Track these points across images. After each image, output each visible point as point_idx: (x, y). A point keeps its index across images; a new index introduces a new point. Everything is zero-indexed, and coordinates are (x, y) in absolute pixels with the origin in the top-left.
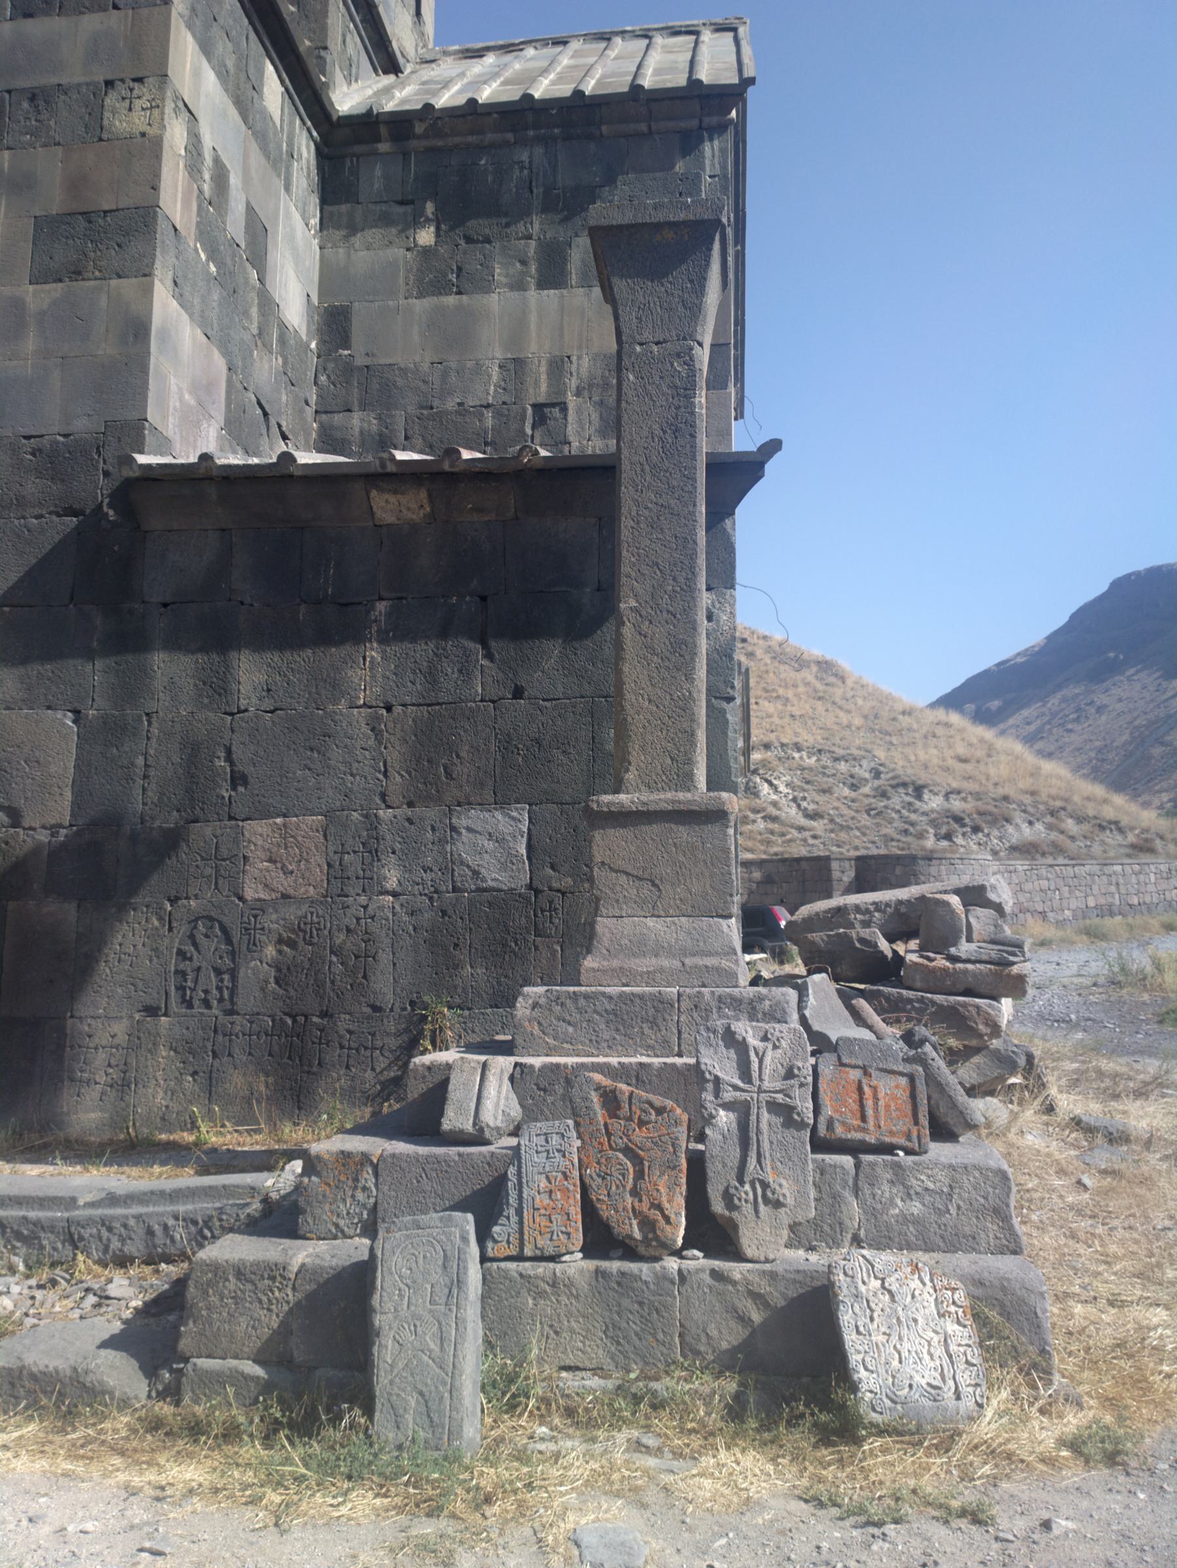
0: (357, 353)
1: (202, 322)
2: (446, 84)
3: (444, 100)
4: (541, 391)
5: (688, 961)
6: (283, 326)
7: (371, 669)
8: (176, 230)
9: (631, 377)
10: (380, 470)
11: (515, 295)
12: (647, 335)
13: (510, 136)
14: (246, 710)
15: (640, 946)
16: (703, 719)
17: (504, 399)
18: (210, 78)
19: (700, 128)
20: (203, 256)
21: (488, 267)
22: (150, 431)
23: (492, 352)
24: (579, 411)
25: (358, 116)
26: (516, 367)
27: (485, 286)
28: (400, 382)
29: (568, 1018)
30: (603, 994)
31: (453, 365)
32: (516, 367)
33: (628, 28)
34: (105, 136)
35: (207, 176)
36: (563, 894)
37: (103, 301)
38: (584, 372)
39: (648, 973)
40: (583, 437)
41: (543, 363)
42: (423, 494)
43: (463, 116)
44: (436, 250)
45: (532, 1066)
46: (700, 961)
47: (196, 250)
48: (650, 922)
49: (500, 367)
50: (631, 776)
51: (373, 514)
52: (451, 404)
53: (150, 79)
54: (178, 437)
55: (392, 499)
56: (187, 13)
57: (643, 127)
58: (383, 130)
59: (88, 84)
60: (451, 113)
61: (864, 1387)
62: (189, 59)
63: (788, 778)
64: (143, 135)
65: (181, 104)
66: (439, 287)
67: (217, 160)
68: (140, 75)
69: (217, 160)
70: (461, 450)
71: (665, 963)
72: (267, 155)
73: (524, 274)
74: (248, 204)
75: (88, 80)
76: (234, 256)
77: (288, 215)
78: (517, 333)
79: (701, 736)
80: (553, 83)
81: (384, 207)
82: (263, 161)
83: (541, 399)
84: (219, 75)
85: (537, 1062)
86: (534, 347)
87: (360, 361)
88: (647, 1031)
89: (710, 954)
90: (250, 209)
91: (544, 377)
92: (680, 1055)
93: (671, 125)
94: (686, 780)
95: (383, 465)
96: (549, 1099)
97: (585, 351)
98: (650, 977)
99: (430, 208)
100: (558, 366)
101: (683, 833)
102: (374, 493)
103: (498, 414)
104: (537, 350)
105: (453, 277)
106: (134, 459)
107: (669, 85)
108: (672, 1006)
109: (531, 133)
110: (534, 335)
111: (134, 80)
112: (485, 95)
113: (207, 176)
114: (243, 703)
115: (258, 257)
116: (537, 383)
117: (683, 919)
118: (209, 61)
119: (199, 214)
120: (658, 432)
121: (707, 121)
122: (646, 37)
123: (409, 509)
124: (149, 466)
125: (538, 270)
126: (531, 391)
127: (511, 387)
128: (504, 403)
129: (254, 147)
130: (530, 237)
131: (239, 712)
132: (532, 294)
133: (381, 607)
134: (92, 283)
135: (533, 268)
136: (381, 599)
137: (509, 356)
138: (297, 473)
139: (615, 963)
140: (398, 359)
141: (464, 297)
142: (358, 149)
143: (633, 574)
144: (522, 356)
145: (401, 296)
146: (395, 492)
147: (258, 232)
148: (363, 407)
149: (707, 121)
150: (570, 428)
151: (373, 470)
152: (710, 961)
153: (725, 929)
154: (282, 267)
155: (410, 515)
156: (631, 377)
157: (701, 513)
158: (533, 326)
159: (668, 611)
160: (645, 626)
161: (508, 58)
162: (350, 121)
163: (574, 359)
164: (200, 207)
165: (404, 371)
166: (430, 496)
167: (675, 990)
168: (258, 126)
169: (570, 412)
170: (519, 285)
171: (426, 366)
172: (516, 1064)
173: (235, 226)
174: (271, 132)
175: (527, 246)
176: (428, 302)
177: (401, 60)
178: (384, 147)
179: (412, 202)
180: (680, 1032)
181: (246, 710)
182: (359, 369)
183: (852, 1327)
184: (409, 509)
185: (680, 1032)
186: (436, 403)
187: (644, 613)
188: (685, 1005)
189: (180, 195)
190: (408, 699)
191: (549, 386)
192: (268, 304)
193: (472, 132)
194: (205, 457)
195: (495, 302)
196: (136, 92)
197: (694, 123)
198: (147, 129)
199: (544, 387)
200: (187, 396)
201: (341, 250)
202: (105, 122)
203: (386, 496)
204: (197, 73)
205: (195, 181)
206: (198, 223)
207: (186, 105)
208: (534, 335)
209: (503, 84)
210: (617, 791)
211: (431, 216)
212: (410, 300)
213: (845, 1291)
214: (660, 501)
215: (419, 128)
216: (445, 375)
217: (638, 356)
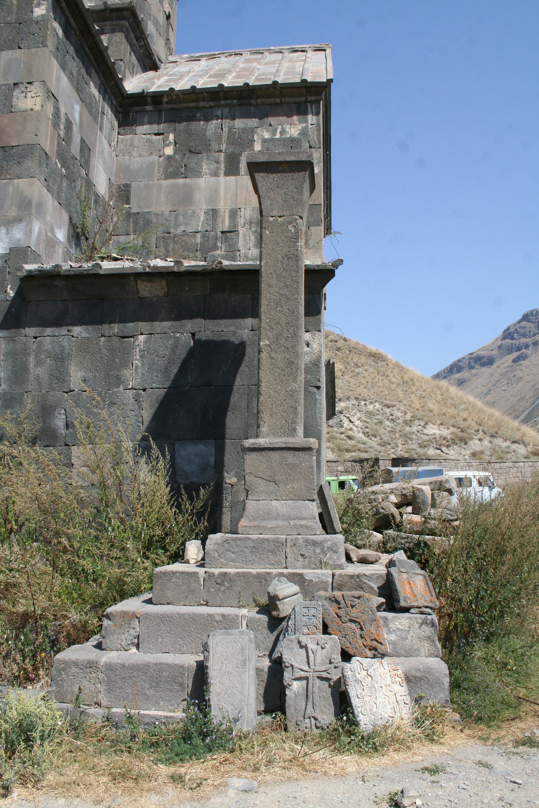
0: (134, 207)
1: (58, 197)
2: (181, 76)
3: (179, 86)
4: (226, 226)
5: (292, 522)
6: (97, 195)
7: (136, 370)
8: (47, 154)
9: (267, 232)
10: (142, 271)
11: (214, 179)
12: (275, 213)
13: (212, 104)
14: (74, 391)
15: (268, 515)
16: (302, 402)
17: (207, 229)
18: (65, 81)
19: (306, 101)
20: (59, 166)
21: (199, 165)
22: (31, 252)
23: (202, 207)
24: (244, 235)
25: (137, 94)
26: (214, 213)
27: (197, 174)
28: (154, 220)
29: (232, 550)
30: (249, 539)
31: (182, 212)
32: (214, 213)
33: (272, 48)
34: (13, 110)
35: (62, 127)
36: (232, 486)
37: (11, 189)
38: (248, 216)
39: (272, 528)
40: (246, 253)
41: (227, 211)
42: (164, 283)
43: (189, 94)
44: (174, 157)
45: (213, 574)
46: (298, 522)
47: (56, 163)
48: (274, 503)
49: (205, 213)
50: (264, 429)
51: (138, 292)
52: (179, 231)
53: (36, 83)
54: (44, 254)
55: (149, 285)
56: (54, 50)
57: (278, 100)
58: (149, 99)
59: (5, 85)
60: (184, 92)
61: (362, 723)
62: (55, 73)
63: (358, 415)
64: (32, 110)
65: (50, 94)
66: (175, 175)
67: (67, 120)
68: (31, 81)
69: (67, 120)
70: (183, 261)
71: (280, 523)
72: (91, 114)
73: (217, 168)
74: (82, 138)
75: (5, 83)
76: (74, 164)
77: (101, 142)
78: (214, 196)
79: (301, 410)
80: (234, 78)
81: (148, 136)
82: (89, 117)
83: (226, 229)
84: (69, 79)
85: (216, 571)
86: (222, 204)
87: (134, 211)
88: (270, 557)
89: (302, 519)
90: (83, 141)
91: (227, 218)
92: (286, 568)
93: (291, 99)
94: (292, 432)
95: (144, 269)
96: (222, 589)
97: (248, 206)
98: (272, 530)
99: (171, 137)
100: (234, 214)
101: (290, 457)
102: (139, 282)
103: (204, 236)
104: (224, 206)
105: (183, 170)
106: (23, 267)
107: (291, 81)
108: (283, 544)
109: (222, 102)
110: (222, 198)
111: (28, 83)
112: (201, 84)
113: (62, 127)
114: (72, 387)
115: (86, 165)
116: (223, 222)
117: (290, 501)
118: (64, 72)
119: (58, 146)
120: (280, 259)
121: (309, 98)
122: (281, 52)
123: (156, 289)
124: (30, 271)
125: (226, 167)
126: (220, 225)
127: (210, 223)
128: (207, 231)
129: (86, 111)
130: (221, 151)
131: (71, 391)
132: (222, 179)
133: (141, 338)
134: (5, 181)
135: (222, 166)
136: (142, 334)
137: (210, 208)
138: (102, 272)
139: (256, 523)
140: (153, 209)
141: (188, 180)
142: (137, 108)
143: (268, 328)
144: (216, 208)
145: (156, 179)
146: (150, 281)
147: (86, 149)
148: (135, 232)
149: (309, 98)
150: (240, 243)
151: (139, 271)
152: (303, 522)
153: (311, 507)
154: (97, 167)
155: (157, 293)
156: (267, 232)
157: (301, 298)
158: (222, 193)
159: (285, 347)
160: (273, 354)
161: (212, 62)
162: (134, 96)
163: (243, 210)
164: (58, 142)
165: (156, 215)
166: (167, 283)
167: (284, 537)
168: (88, 101)
169: (240, 235)
170: (215, 174)
171: (167, 213)
172: (206, 572)
173: (75, 149)
174: (94, 103)
175: (219, 155)
176: (170, 182)
177: (159, 63)
178: (149, 108)
179: (162, 134)
180: (286, 557)
181: (74, 391)
182: (133, 214)
183: (355, 696)
184: (156, 289)
185: (286, 557)
186: (172, 230)
187: (272, 347)
188: (289, 544)
189: (49, 138)
190: (154, 385)
191: (230, 222)
192: (89, 184)
193: (194, 101)
194: (57, 266)
195: (203, 183)
196: (28, 89)
197: (303, 99)
198: (34, 107)
199: (227, 223)
200: (49, 234)
201: (127, 157)
202: (14, 103)
203: (146, 283)
204: (58, 79)
205: (56, 130)
206: (57, 151)
207: (53, 95)
208: (222, 198)
209: (209, 77)
210: (257, 436)
211: (172, 141)
212: (160, 181)
213: (351, 679)
214: (281, 292)
215: (165, 99)
216: (177, 217)
217: (271, 222)
